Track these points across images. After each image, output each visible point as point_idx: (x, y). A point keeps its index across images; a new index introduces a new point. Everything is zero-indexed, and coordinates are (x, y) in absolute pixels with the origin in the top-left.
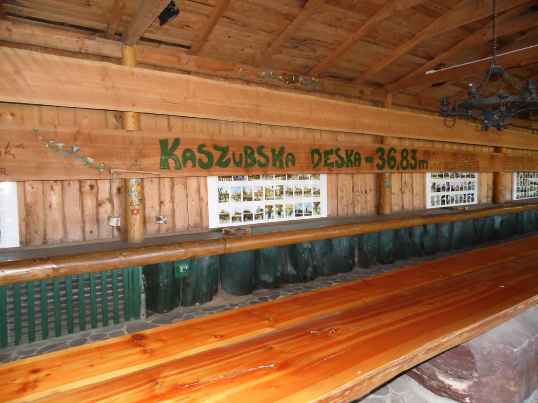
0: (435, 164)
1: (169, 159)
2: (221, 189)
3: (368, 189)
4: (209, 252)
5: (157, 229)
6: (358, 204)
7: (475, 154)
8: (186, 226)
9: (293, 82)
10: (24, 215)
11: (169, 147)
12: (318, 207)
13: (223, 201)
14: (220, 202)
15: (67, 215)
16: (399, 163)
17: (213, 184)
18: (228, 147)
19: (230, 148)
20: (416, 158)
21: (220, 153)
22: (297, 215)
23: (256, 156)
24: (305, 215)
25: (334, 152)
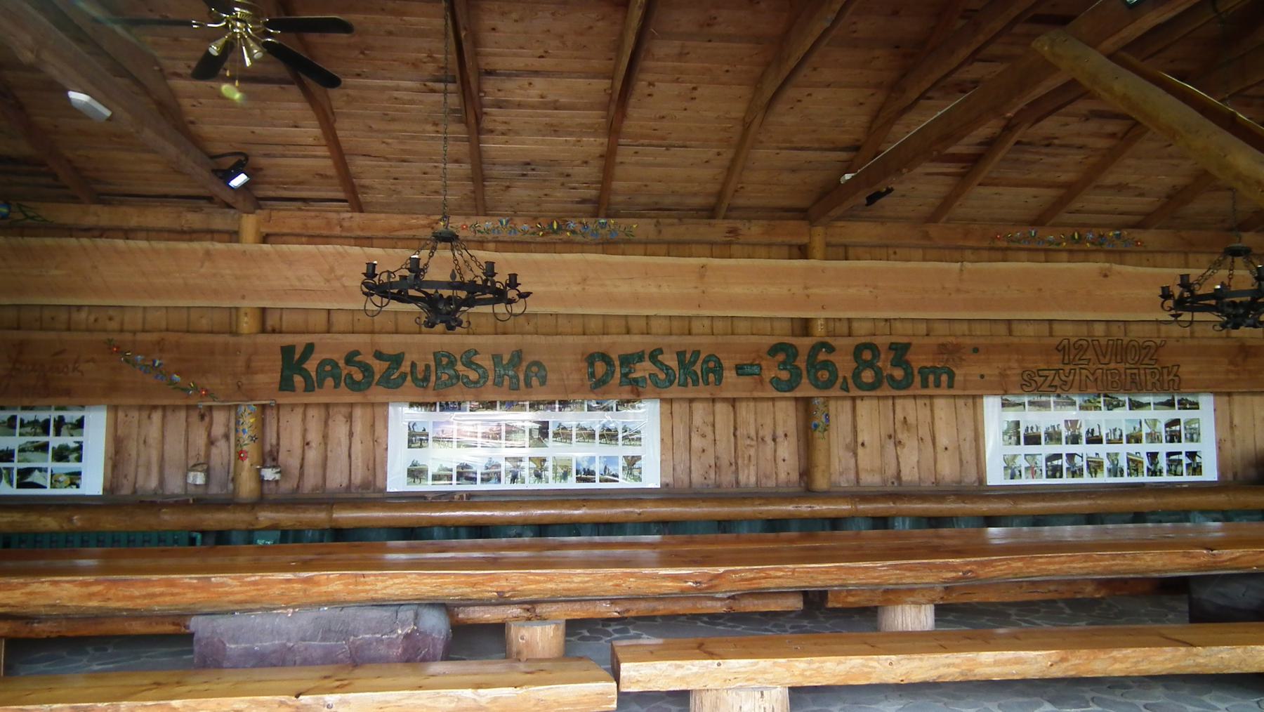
0: (982, 376)
1: (295, 376)
2: (414, 424)
3: (780, 432)
4: (300, 522)
5: (295, 486)
6: (748, 466)
7: (1158, 348)
8: (344, 485)
9: (555, 232)
10: (112, 450)
11: (297, 356)
12: (636, 466)
13: (416, 445)
14: (409, 447)
15: (166, 455)
16: (849, 375)
17: (402, 416)
18: (403, 353)
19: (407, 356)
20: (908, 363)
21: (385, 365)
22: (579, 480)
23: (460, 367)
24: (600, 481)
25: (647, 356)
